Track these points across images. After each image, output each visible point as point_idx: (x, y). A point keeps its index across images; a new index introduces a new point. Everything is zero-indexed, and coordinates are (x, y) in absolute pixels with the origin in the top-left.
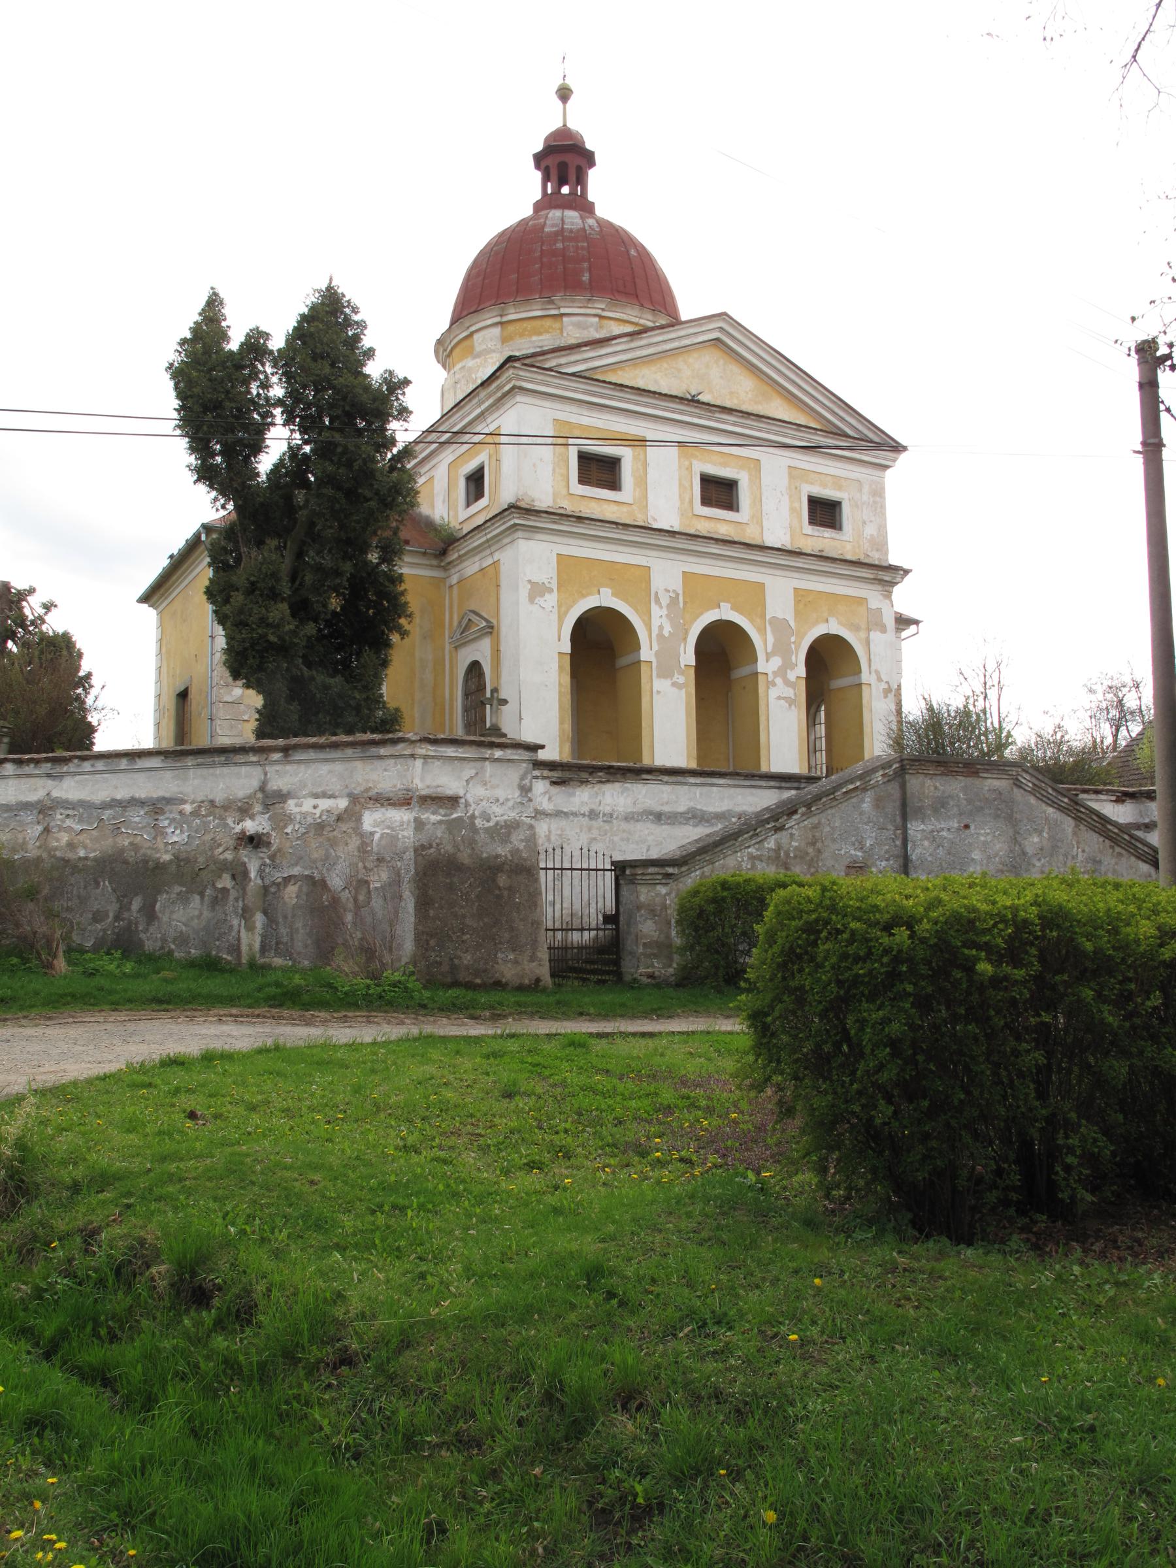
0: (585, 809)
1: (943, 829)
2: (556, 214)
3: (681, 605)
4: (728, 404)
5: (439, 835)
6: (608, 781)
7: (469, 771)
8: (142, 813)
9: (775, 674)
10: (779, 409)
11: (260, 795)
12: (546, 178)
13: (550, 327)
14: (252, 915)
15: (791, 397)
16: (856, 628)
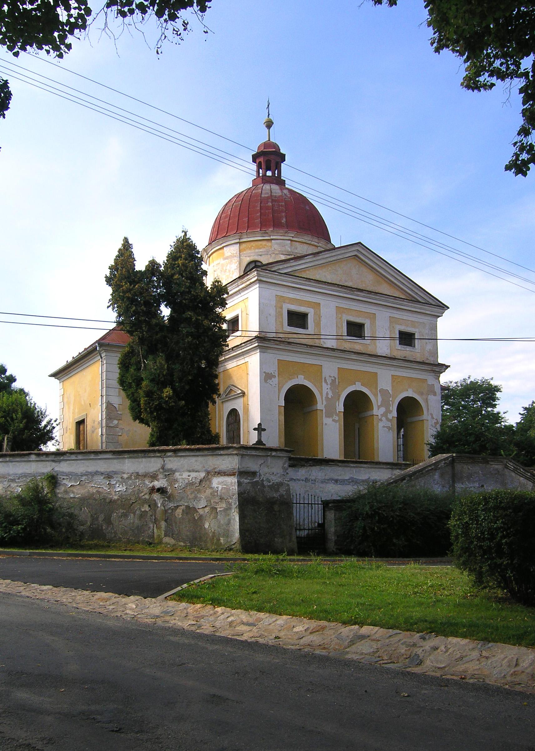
0: (303, 478)
1: (471, 487)
2: (267, 187)
3: (337, 383)
4: (360, 287)
5: (248, 488)
6: (314, 465)
7: (261, 461)
8: (102, 478)
9: (382, 415)
10: (385, 289)
11: (161, 470)
12: (259, 167)
13: (265, 245)
14: (159, 523)
15: (390, 282)
16: (421, 394)
